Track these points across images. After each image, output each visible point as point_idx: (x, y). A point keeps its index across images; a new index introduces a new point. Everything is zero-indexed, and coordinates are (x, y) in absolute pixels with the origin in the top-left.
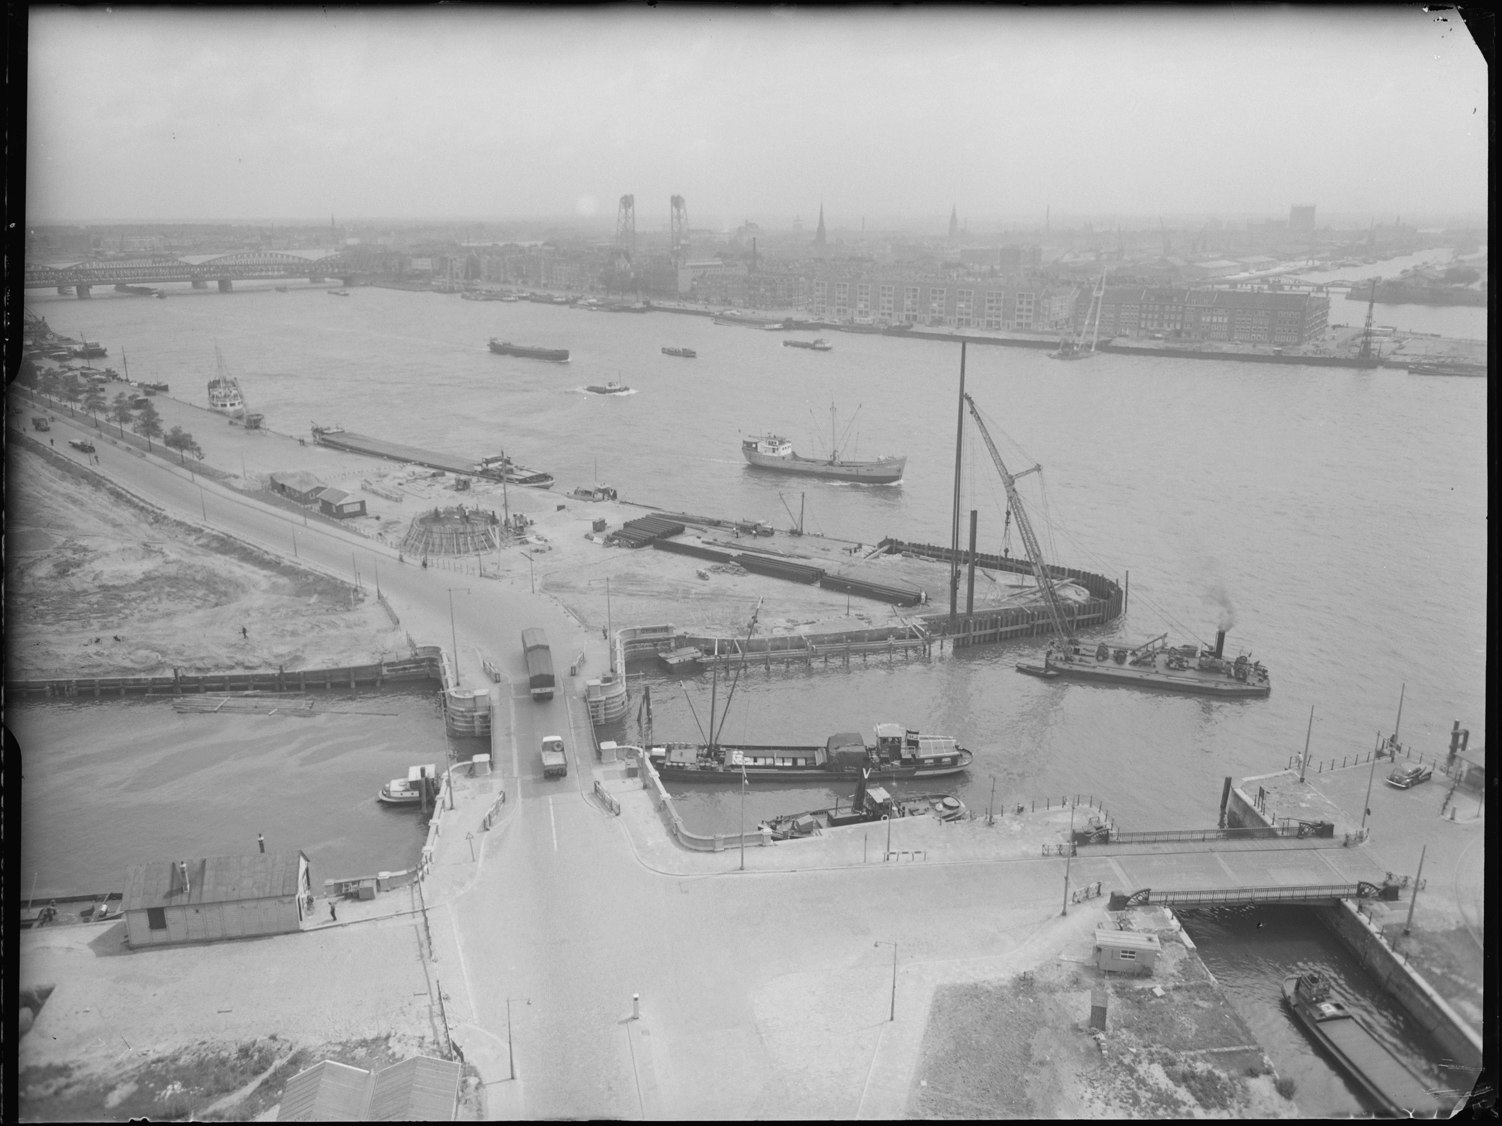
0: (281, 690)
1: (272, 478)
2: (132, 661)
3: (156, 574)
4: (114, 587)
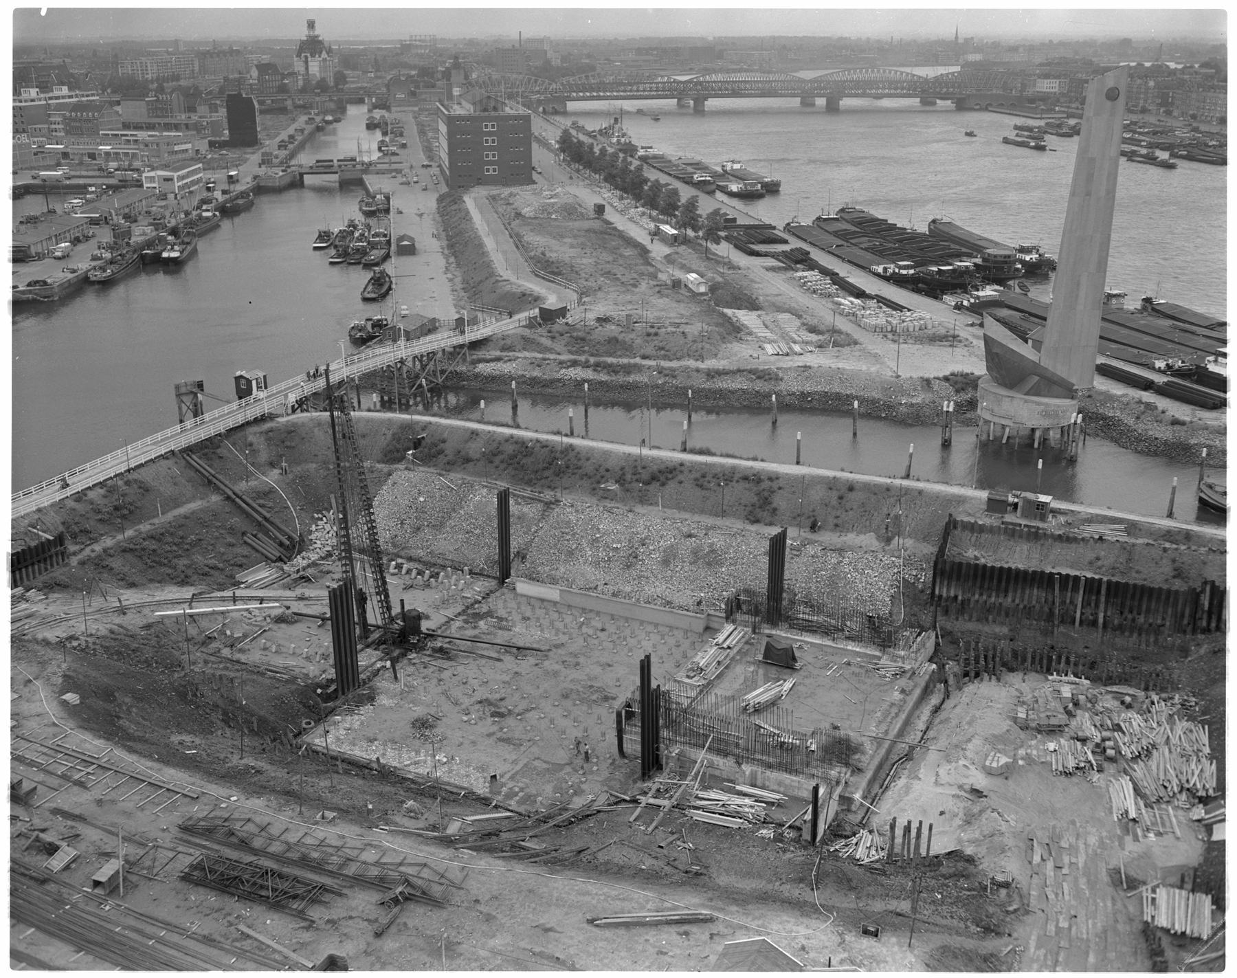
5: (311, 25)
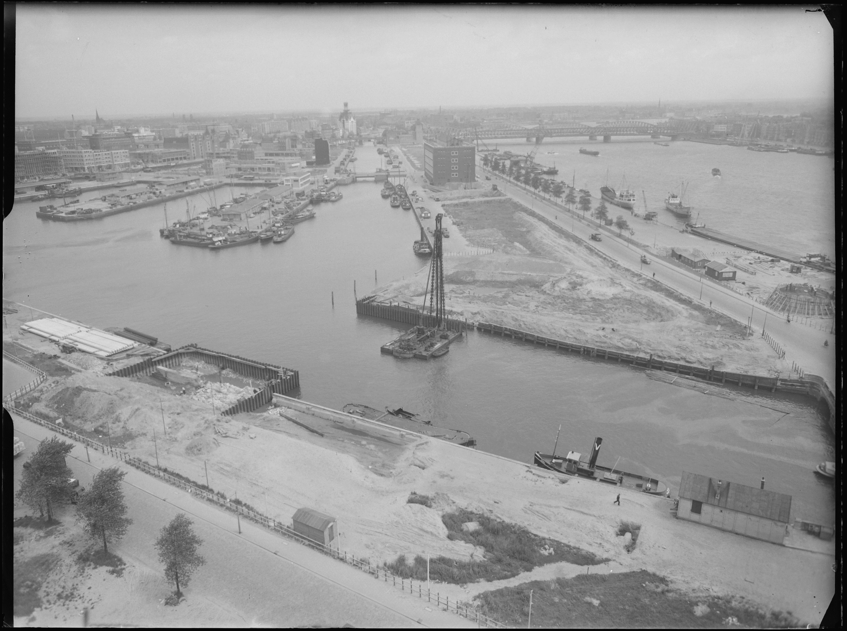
0: (710, 379)
1: (673, 251)
2: (622, 344)
3: (620, 296)
4: (599, 300)
5: (346, 105)
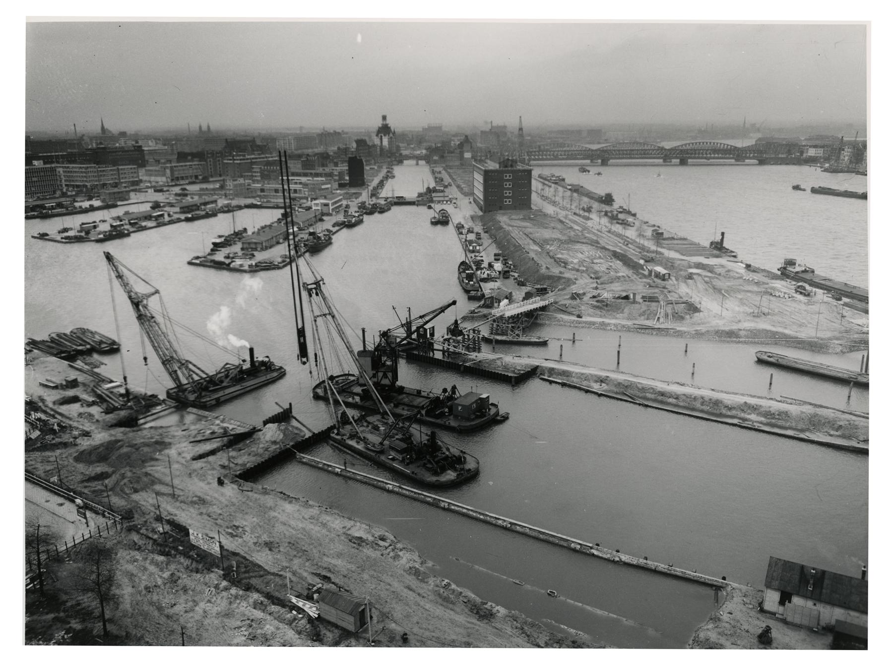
5: (384, 118)
